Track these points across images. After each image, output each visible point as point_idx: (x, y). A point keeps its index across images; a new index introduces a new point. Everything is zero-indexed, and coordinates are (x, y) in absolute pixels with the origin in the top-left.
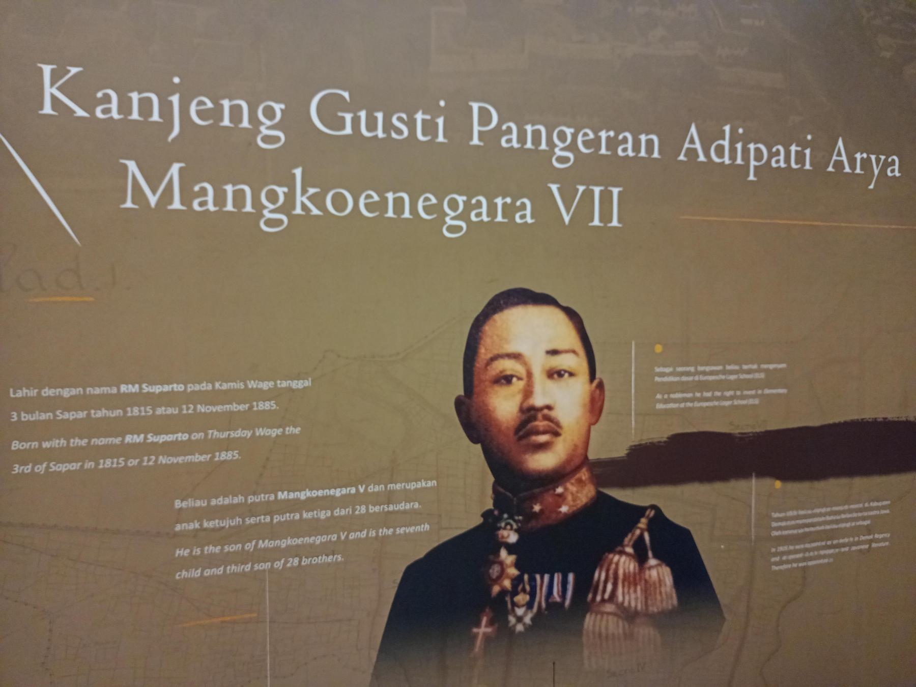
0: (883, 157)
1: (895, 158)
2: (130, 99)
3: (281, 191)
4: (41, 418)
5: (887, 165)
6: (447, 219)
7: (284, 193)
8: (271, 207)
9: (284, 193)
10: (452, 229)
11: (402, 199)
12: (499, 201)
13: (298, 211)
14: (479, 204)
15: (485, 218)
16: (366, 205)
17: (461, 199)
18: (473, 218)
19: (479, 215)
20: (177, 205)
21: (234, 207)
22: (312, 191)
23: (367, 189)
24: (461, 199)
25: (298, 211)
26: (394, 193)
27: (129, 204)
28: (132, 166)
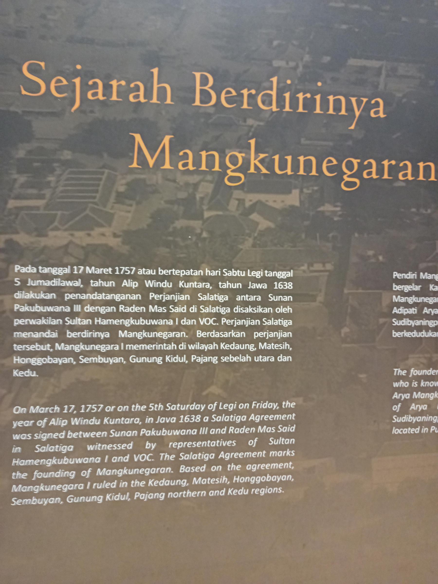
0: (365, 100)
1: (372, 161)
2: (328, 100)
3: (240, 156)
4: (25, 297)
5: (368, 107)
6: (345, 177)
7: (358, 163)
8: (233, 168)
9: (358, 163)
10: (348, 184)
11: (310, 161)
12: (386, 163)
13: (252, 170)
14: (370, 166)
15: (374, 176)
16: (328, 168)
17: (355, 162)
18: (365, 176)
19: (369, 173)
20: (167, 166)
21: (207, 167)
22: (262, 156)
23: (328, 157)
24: (355, 162)
25: (252, 170)
26: (207, 152)
27: (135, 165)
28: (138, 137)
